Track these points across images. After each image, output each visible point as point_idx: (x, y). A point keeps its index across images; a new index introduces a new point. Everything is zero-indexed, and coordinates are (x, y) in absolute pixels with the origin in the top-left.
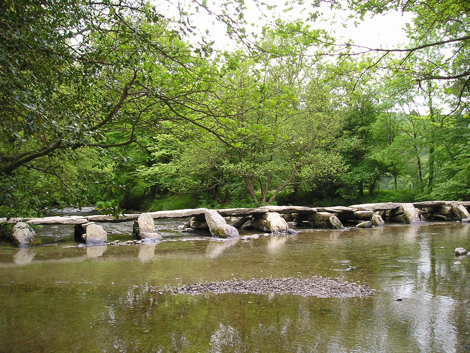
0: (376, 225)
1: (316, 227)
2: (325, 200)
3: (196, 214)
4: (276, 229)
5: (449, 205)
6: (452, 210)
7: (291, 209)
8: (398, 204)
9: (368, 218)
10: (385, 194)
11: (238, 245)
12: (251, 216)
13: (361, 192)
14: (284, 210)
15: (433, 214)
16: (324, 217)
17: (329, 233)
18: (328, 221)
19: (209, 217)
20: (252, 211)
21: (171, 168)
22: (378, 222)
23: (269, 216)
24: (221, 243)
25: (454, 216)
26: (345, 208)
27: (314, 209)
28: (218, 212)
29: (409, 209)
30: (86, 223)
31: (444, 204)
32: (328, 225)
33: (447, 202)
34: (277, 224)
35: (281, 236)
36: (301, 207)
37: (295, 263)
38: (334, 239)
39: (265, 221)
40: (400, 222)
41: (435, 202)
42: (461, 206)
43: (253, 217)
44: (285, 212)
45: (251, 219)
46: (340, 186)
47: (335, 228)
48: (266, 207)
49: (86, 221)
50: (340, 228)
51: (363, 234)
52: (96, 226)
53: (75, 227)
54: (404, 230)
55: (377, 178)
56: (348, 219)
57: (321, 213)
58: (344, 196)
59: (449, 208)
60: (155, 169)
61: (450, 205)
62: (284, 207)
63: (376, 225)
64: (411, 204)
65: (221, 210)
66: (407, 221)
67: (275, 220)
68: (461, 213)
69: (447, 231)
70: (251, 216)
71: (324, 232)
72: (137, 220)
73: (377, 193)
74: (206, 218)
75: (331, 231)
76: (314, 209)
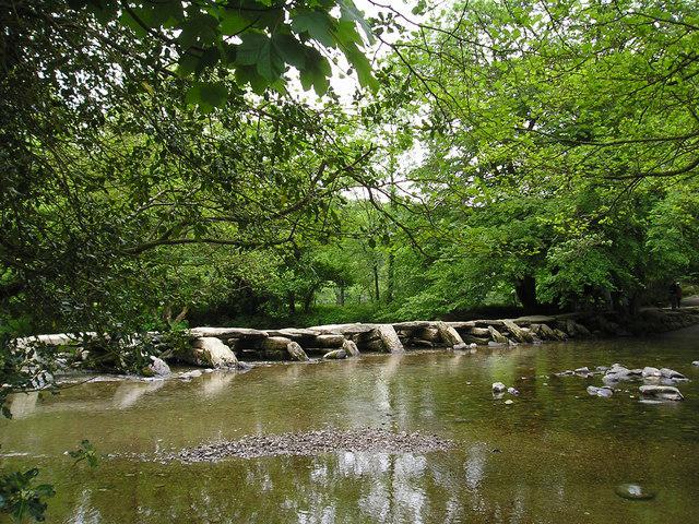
0: (350, 355)
1: (265, 358)
2: (240, 319)
4: (221, 362)
5: (435, 327)
6: (439, 334)
8: (372, 326)
9: (337, 345)
10: (329, 311)
11: (167, 387)
13: (292, 307)
14: (217, 333)
15: (414, 339)
16: (279, 343)
17: (286, 368)
18: (286, 349)
22: (352, 352)
24: (141, 384)
25: (442, 341)
27: (265, 332)
29: (388, 331)
31: (428, 325)
32: (286, 356)
33: (432, 323)
35: (229, 372)
37: (231, 408)
38: (292, 376)
40: (375, 350)
41: (418, 322)
42: (450, 328)
46: (264, 300)
47: (296, 359)
50: (304, 360)
51: (336, 368)
54: (382, 361)
55: (316, 287)
56: (313, 346)
58: (271, 313)
59: (435, 331)
61: (436, 326)
62: (222, 330)
63: (350, 355)
64: (390, 326)
66: (386, 349)
67: (218, 350)
68: (451, 337)
69: (434, 364)
71: (263, 368)
73: (317, 310)
75: (118, 384)
76: (265, 332)
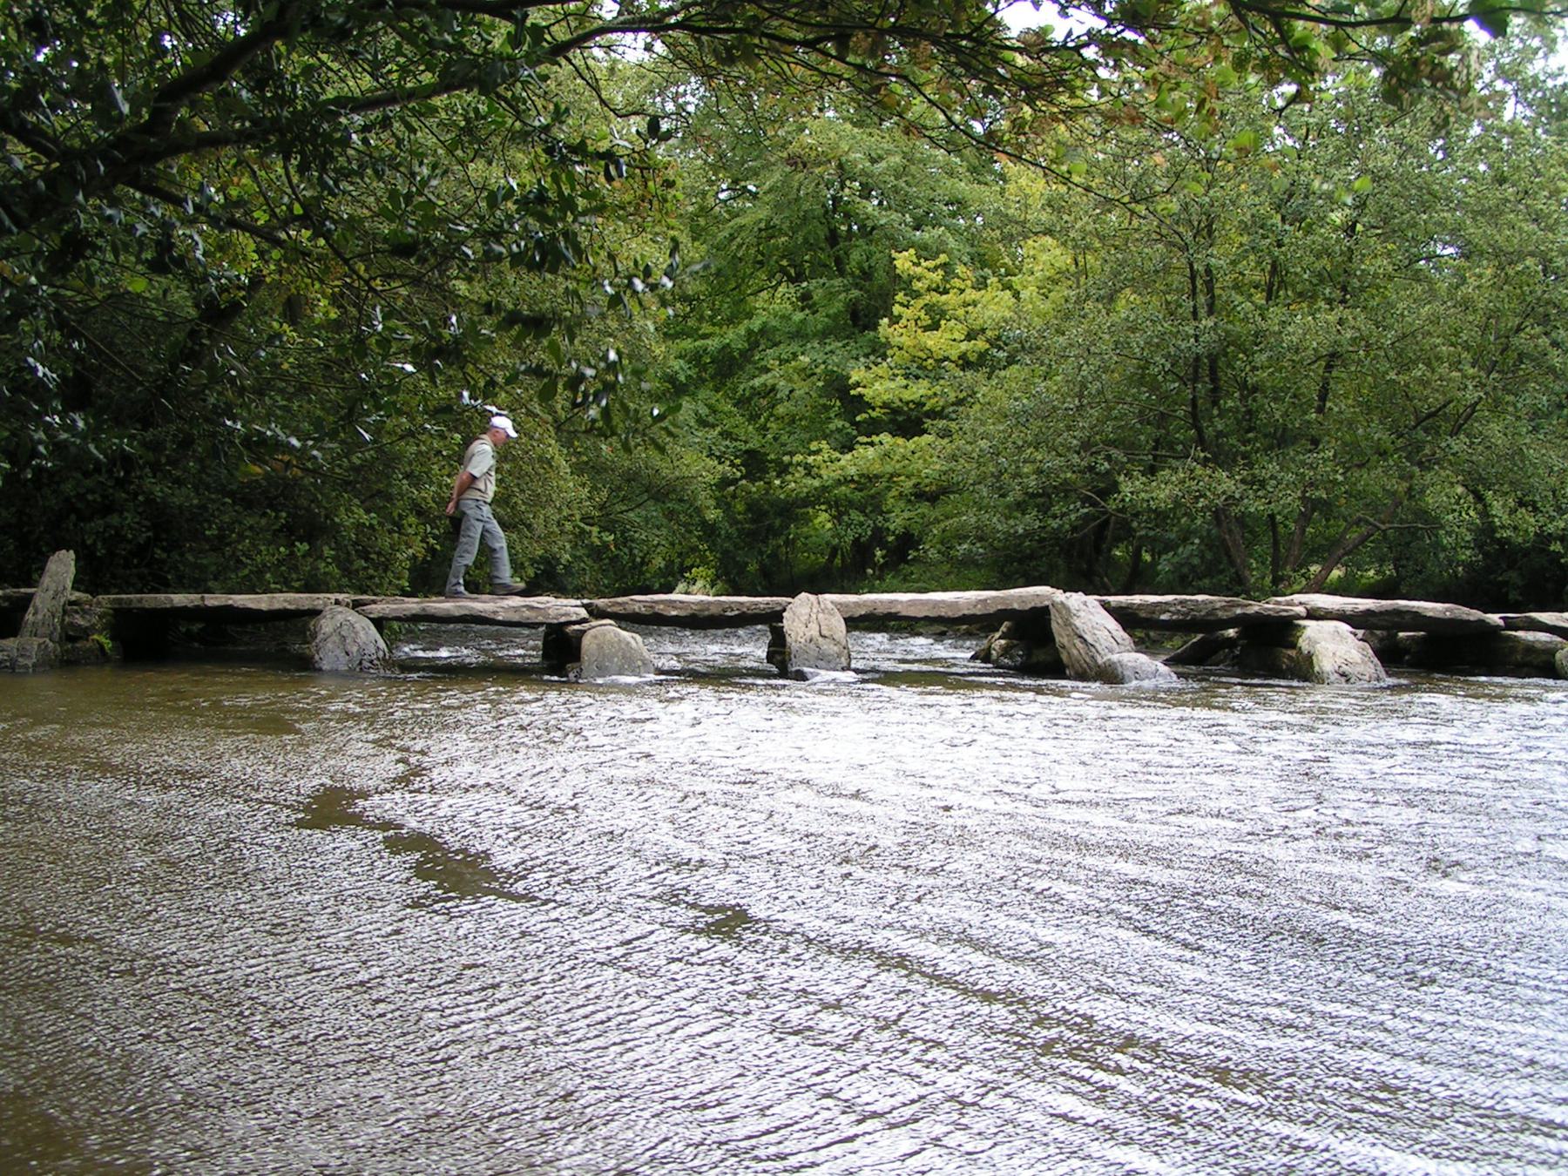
3: (1014, 610)
7: (1398, 612)
12: (1231, 632)
14: (1369, 612)
19: (1068, 623)
20: (1239, 611)
21: (924, 456)
23: (1307, 633)
26: (1475, 615)
28: (1106, 606)
30: (584, 621)
34: (1339, 661)
36: (1439, 606)
39: (1292, 653)
43: (1240, 635)
44: (1373, 620)
45: (1231, 642)
48: (1297, 598)
49: (583, 613)
52: (616, 635)
53: (547, 635)
57: (1520, 634)
60: (865, 457)
64: (1092, 600)
65: (1114, 600)
70: (1231, 632)
72: (781, 619)
74: (1054, 625)
76: (1495, 618)
